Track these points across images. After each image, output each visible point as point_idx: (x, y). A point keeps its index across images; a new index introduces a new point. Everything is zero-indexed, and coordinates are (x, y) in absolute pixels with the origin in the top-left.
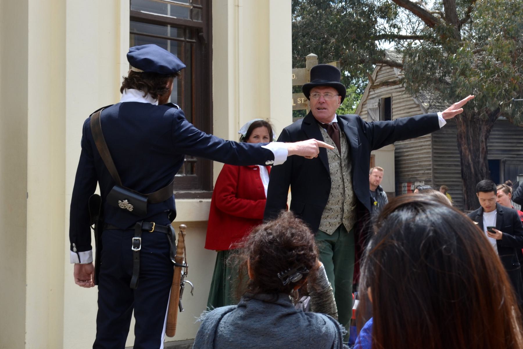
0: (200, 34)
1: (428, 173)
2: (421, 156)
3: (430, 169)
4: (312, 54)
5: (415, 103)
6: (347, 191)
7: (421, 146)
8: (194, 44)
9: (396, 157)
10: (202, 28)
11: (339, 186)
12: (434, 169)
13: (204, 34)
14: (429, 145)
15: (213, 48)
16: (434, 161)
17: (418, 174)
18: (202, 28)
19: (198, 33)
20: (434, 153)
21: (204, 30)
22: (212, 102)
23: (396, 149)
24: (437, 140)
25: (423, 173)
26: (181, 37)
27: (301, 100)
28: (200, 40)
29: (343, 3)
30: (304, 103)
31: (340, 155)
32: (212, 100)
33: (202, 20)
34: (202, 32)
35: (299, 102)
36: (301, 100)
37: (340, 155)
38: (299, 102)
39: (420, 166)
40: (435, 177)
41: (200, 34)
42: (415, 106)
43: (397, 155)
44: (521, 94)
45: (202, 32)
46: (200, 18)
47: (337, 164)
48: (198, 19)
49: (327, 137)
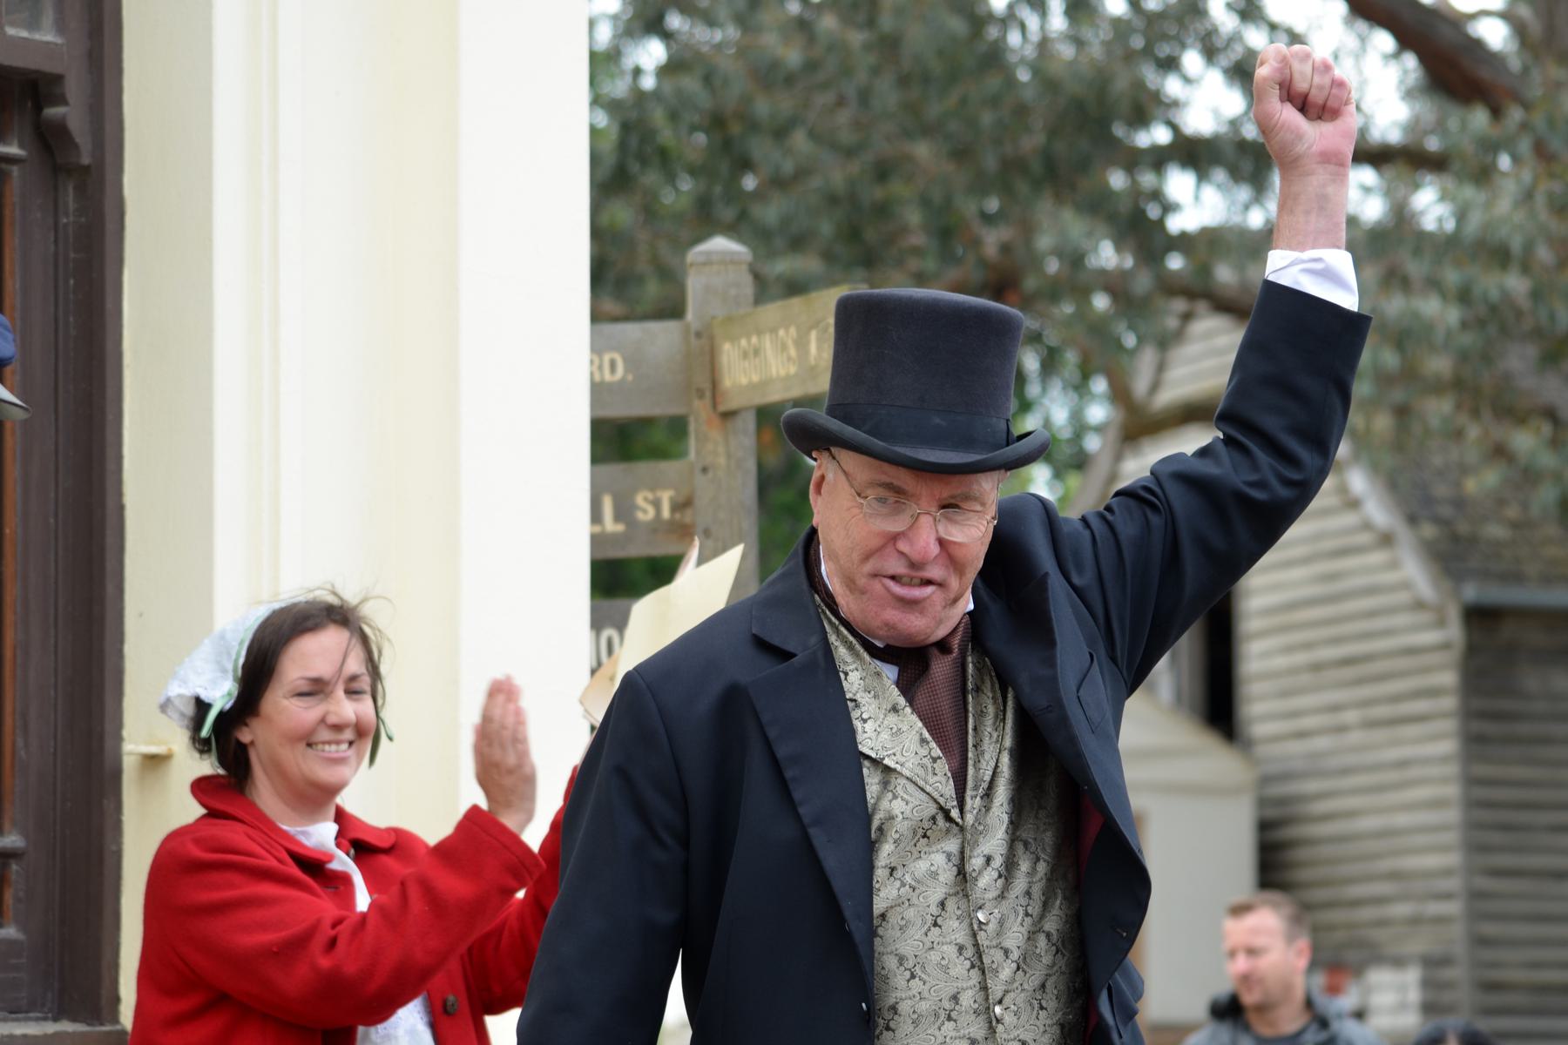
0: (52, 112)
1: (1440, 920)
2: (1402, 820)
3: (1447, 896)
4: (720, 244)
5: (1367, 526)
6: (1009, 1019)
7: (1403, 764)
8: (15, 170)
9: (1265, 826)
10: (58, 79)
11: (955, 998)
12: (1475, 895)
13: (71, 113)
14: (1444, 759)
15: (128, 191)
16: (1474, 848)
17: (1382, 923)
18: (58, 79)
19: (38, 109)
20: (1471, 804)
21: (75, 88)
22: (121, 508)
23: (1266, 780)
24: (1490, 728)
25: (1415, 921)
26: (10, 144)
27: (657, 504)
28: (51, 143)
29: (1058, 21)
30: (671, 522)
31: (962, 812)
32: (119, 493)
33: (61, 27)
34: (63, 101)
35: (646, 514)
36: (657, 504)
37: (962, 812)
38: (646, 514)
39: (1395, 876)
40: (1482, 942)
41: (52, 112)
42: (1364, 538)
43: (1272, 813)
44: (1562, 350)
45: (63, 101)
46: (48, 17)
47: (939, 859)
48: (33, 24)
49: (895, 709)
